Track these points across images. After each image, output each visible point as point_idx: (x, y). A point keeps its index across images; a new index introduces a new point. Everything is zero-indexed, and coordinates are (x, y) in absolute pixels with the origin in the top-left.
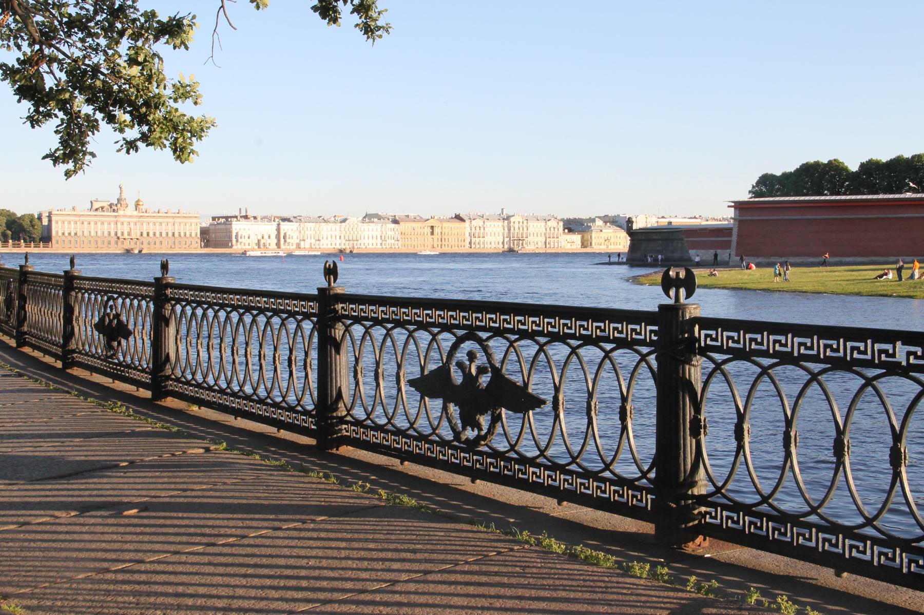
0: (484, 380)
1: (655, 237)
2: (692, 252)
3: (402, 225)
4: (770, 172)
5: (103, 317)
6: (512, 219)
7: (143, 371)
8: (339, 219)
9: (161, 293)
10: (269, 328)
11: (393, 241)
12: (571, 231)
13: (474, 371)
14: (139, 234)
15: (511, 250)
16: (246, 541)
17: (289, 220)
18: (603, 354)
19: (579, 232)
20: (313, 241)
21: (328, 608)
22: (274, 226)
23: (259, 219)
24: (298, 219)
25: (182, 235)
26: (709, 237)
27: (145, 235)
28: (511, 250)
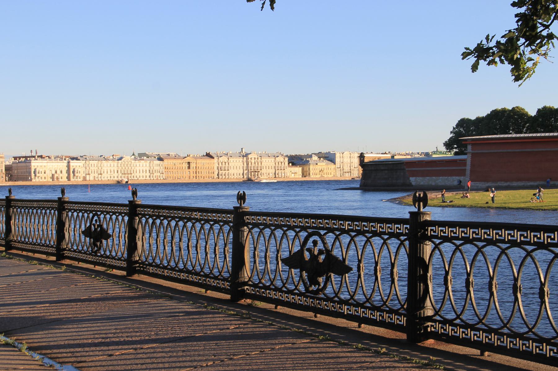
0: (322, 257)
1: (382, 168)
2: (412, 179)
3: (166, 161)
4: (466, 117)
5: (90, 226)
6: (250, 156)
7: (224, 279)
8: (117, 158)
9: (133, 209)
10: (185, 229)
11: (159, 174)
12: (294, 164)
13: (316, 253)
15: (249, 180)
16: (295, 346)
17: (77, 159)
18: (382, 241)
19: (300, 165)
20: (96, 175)
22: (65, 163)
23: (53, 158)
24: (83, 158)
26: (425, 166)
28: (249, 180)
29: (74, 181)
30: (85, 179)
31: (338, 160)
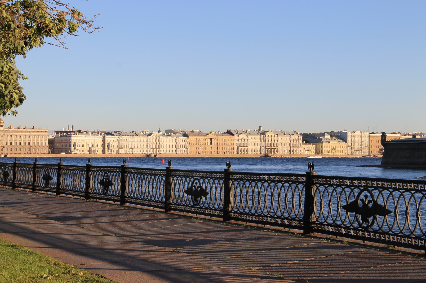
0: (371, 205)
6: (267, 134)
8: (146, 133)
11: (184, 149)
12: (308, 142)
13: (366, 202)
14: (4, 144)
15: (266, 156)
17: (111, 134)
19: (313, 143)
20: (128, 149)
21: (319, 278)
22: (100, 138)
23: (90, 133)
25: (36, 144)
27: (9, 144)
28: (266, 156)
29: (107, 154)
30: (118, 152)
31: (349, 139)
